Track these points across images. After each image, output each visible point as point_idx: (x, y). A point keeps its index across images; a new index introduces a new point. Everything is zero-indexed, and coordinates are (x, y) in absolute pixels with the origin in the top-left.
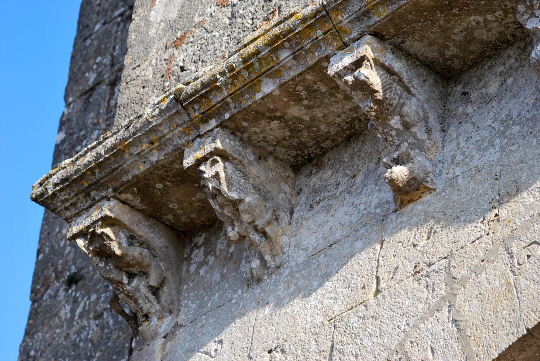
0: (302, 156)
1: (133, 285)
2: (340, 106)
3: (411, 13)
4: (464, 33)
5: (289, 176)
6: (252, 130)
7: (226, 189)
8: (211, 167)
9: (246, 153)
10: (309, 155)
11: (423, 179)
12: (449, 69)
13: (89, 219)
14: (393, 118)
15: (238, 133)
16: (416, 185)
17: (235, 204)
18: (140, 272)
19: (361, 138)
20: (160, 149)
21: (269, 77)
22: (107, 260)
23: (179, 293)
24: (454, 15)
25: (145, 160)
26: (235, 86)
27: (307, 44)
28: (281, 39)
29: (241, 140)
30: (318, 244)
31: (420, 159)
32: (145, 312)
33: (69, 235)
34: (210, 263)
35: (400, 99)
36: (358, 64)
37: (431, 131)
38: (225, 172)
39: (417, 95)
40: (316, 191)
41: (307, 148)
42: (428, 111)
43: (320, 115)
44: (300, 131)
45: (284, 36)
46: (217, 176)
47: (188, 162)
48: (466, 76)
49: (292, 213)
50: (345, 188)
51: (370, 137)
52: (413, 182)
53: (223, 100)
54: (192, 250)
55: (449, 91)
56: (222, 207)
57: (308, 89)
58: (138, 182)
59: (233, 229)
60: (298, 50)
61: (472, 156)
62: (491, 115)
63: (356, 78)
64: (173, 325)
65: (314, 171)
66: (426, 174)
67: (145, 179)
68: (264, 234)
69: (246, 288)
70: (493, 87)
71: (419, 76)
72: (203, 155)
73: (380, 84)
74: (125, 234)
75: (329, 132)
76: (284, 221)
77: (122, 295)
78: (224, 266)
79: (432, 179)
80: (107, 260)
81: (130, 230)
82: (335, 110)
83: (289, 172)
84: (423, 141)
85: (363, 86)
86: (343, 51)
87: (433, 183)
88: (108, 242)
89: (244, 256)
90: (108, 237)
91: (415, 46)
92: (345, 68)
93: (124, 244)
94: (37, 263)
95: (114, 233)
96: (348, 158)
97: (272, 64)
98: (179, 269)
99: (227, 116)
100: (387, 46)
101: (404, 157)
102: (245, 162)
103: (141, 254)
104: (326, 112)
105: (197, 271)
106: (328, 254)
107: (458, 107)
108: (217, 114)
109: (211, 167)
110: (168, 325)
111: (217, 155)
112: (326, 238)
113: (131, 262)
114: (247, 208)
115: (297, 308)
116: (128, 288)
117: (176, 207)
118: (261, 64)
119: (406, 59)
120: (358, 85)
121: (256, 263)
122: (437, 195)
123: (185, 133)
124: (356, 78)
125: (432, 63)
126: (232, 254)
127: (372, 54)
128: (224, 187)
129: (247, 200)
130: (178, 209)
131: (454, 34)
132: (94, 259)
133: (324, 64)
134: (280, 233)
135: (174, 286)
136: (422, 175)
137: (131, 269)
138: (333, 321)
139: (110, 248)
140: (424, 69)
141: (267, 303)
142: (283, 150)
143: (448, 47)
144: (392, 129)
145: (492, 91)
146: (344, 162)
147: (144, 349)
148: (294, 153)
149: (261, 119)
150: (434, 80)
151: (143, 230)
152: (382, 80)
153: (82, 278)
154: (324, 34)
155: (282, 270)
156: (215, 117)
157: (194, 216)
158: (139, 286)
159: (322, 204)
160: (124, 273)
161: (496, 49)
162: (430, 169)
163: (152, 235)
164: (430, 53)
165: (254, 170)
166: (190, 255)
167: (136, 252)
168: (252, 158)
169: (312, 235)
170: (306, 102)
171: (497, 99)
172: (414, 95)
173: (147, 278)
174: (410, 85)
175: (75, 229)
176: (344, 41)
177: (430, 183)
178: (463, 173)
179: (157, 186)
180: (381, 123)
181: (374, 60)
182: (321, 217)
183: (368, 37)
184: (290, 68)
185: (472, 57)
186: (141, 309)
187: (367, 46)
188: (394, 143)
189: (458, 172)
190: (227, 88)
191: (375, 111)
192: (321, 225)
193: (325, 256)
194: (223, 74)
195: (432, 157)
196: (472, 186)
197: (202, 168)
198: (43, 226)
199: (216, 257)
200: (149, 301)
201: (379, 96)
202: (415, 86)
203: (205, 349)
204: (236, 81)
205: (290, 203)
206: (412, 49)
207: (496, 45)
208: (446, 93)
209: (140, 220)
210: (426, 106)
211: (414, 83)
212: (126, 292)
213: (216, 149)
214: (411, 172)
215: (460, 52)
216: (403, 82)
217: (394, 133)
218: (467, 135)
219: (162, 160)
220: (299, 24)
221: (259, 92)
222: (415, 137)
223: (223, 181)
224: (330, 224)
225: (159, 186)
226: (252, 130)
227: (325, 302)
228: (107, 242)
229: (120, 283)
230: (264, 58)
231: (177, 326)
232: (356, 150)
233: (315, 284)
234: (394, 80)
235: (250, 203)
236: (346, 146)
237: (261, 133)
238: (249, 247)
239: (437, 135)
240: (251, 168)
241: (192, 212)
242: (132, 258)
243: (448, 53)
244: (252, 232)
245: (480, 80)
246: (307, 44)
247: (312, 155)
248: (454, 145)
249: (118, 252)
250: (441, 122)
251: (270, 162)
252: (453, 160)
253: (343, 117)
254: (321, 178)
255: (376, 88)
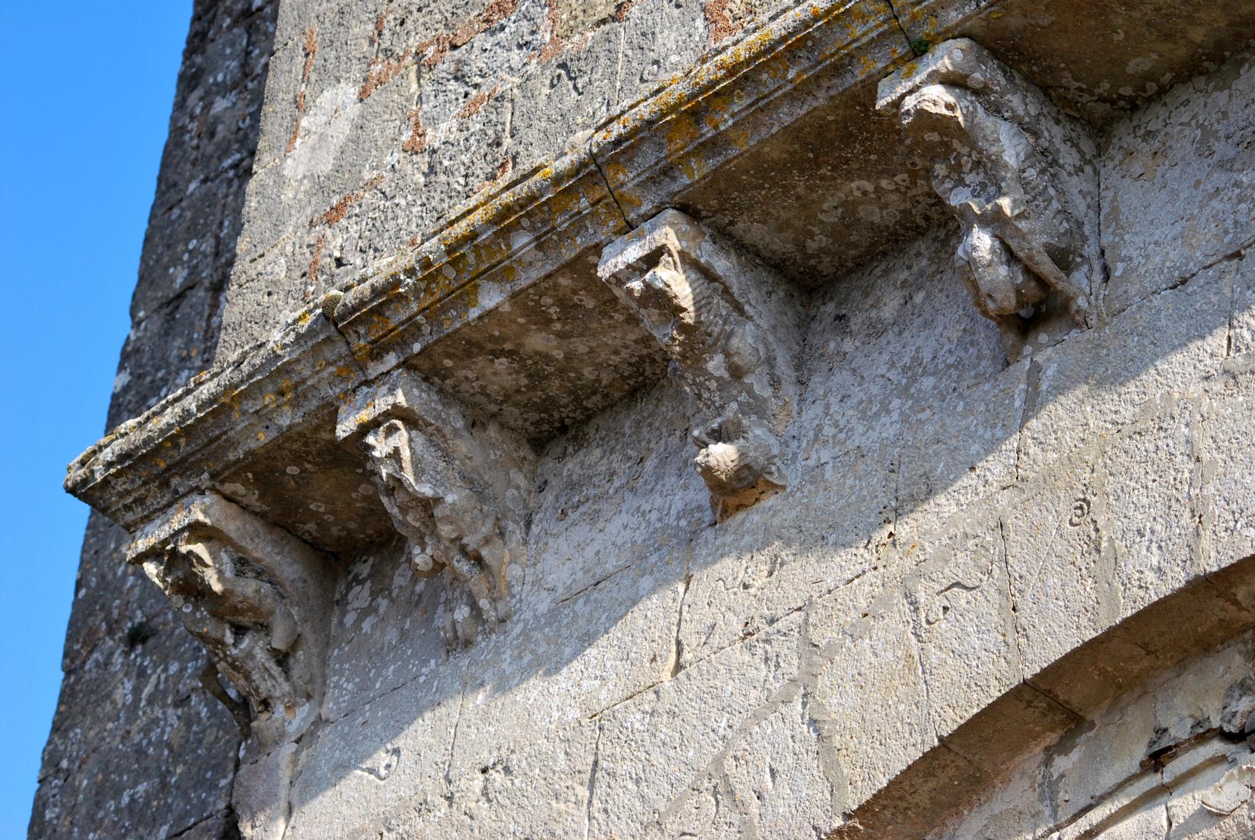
0: (550, 423)
1: (242, 646)
2: (619, 335)
3: (747, 172)
4: (840, 210)
5: (524, 458)
6: (461, 373)
7: (412, 479)
8: (386, 438)
9: (448, 415)
10: (562, 420)
11: (763, 469)
12: (813, 273)
13: (166, 527)
14: (712, 358)
15: (436, 379)
16: (751, 478)
17: (427, 506)
18: (256, 623)
19: (656, 393)
20: (295, 404)
21: (493, 280)
22: (197, 601)
23: (324, 662)
24: (822, 178)
25: (268, 423)
26: (433, 294)
27: (562, 222)
28: (516, 212)
29: (441, 391)
30: (574, 581)
31: (758, 432)
32: (264, 695)
33: (131, 555)
34: (382, 611)
35: (725, 324)
36: (652, 259)
37: (779, 382)
38: (411, 448)
39: (755, 317)
40: (573, 486)
41: (558, 407)
42: (775, 346)
43: (582, 349)
44: (546, 377)
45: (522, 207)
46: (395, 455)
47: (345, 429)
48: (842, 287)
49: (528, 524)
50: (624, 481)
51: (671, 390)
52: (746, 473)
53: (410, 319)
54: (349, 588)
55: (813, 312)
56: (404, 510)
57: (561, 302)
58: (254, 463)
59: (423, 551)
60: (546, 233)
61: (851, 429)
62: (886, 357)
63: (648, 286)
64: (312, 719)
65: (570, 450)
66: (768, 459)
67: (267, 459)
68: (478, 560)
69: (444, 657)
70: (889, 308)
71: (760, 284)
72: (371, 417)
73: (691, 297)
74: (230, 556)
75: (598, 380)
76: (514, 539)
77: (223, 664)
78: (405, 617)
79: (778, 469)
80: (197, 601)
81: (238, 548)
82: (610, 342)
83: (526, 451)
84: (765, 400)
85: (659, 299)
86: (626, 237)
87: (781, 476)
88: (200, 568)
89: (442, 600)
90: (200, 559)
91: (754, 231)
92: (629, 266)
93: (229, 574)
94: (76, 604)
95: (211, 554)
96: (630, 427)
97: (499, 257)
98: (325, 620)
99: (417, 347)
100: (705, 229)
101: (731, 428)
102: (447, 430)
103: (258, 591)
104: (594, 344)
105: (357, 625)
106: (592, 598)
107: (827, 341)
108: (398, 344)
109: (386, 438)
110: (303, 719)
111: (397, 418)
112: (589, 570)
113: (240, 606)
114: (448, 513)
115: (534, 694)
116: (234, 651)
117: (322, 510)
118: (478, 257)
119: (737, 254)
120: (651, 297)
121: (462, 613)
122: (787, 497)
123: (340, 377)
124: (648, 286)
125: (784, 261)
126: (420, 595)
127: (677, 242)
128: (408, 476)
129: (450, 499)
130: (325, 513)
131: (823, 211)
132: (174, 598)
133: (592, 259)
134: (507, 559)
135: (315, 651)
136: (762, 461)
137: (240, 618)
138: (597, 718)
139: (203, 579)
140: (769, 272)
141: (482, 685)
142: (516, 411)
143: (811, 235)
144: (711, 377)
145: (887, 315)
146: (624, 434)
147: (261, 762)
148: (535, 416)
149: (477, 356)
150: (786, 291)
151: (263, 549)
152: (694, 290)
153: (155, 633)
154: (592, 205)
155: (509, 625)
156: (394, 350)
157: (353, 526)
158: (254, 648)
159: (582, 509)
160: (227, 626)
161: (897, 241)
162: (775, 451)
163: (278, 558)
164: (780, 244)
165: (463, 446)
166: (346, 595)
167: (249, 587)
168: (460, 424)
169: (564, 564)
170: (558, 326)
171: (896, 329)
172: (750, 318)
173: (267, 635)
174: (743, 301)
175: (142, 545)
176: (629, 218)
177: (776, 475)
178: (834, 458)
179: (288, 470)
180: (690, 366)
181: (681, 253)
182: (581, 532)
183: (670, 213)
184: (530, 264)
185: (852, 253)
186: (257, 689)
187: (668, 229)
188: (713, 403)
189: (825, 456)
190: (418, 298)
191: (681, 344)
192: (580, 547)
193: (585, 603)
194: (410, 272)
195: (780, 428)
196: (849, 482)
197: (370, 439)
198: (87, 538)
199: (392, 601)
200: (271, 676)
201: (689, 318)
202: (753, 302)
203: (368, 764)
204: (433, 285)
205: (526, 507)
206: (749, 236)
207: (895, 233)
208: (808, 316)
209: (256, 530)
210: (771, 338)
211: (750, 296)
212: (230, 660)
213: (395, 406)
214: (742, 455)
215: (833, 244)
216: (732, 295)
217: (713, 385)
218: (843, 392)
219: (299, 424)
220: (547, 187)
221: (475, 306)
222: (750, 392)
223: (407, 464)
224: (596, 546)
225: (293, 470)
226: (461, 373)
227: (585, 683)
228: (198, 569)
229: (220, 642)
230: (485, 247)
231: (320, 722)
232: (645, 414)
233: (568, 651)
234: (715, 290)
235: (454, 504)
236: (629, 407)
237: (477, 379)
238: (451, 584)
239: (790, 390)
240: (458, 442)
241: (351, 519)
242: (241, 599)
243: (812, 246)
244: (458, 557)
245: (866, 295)
246: (562, 222)
247: (567, 421)
248: (819, 408)
249: (217, 587)
250: (798, 368)
251: (493, 431)
252: (816, 435)
253: (624, 354)
254: (582, 463)
255: (684, 305)
